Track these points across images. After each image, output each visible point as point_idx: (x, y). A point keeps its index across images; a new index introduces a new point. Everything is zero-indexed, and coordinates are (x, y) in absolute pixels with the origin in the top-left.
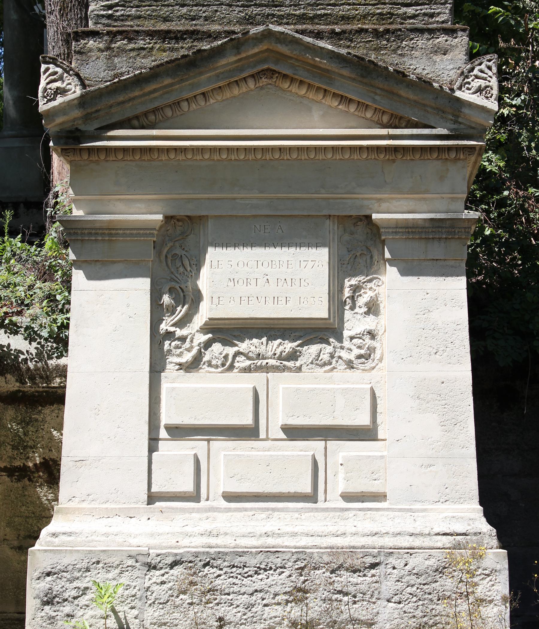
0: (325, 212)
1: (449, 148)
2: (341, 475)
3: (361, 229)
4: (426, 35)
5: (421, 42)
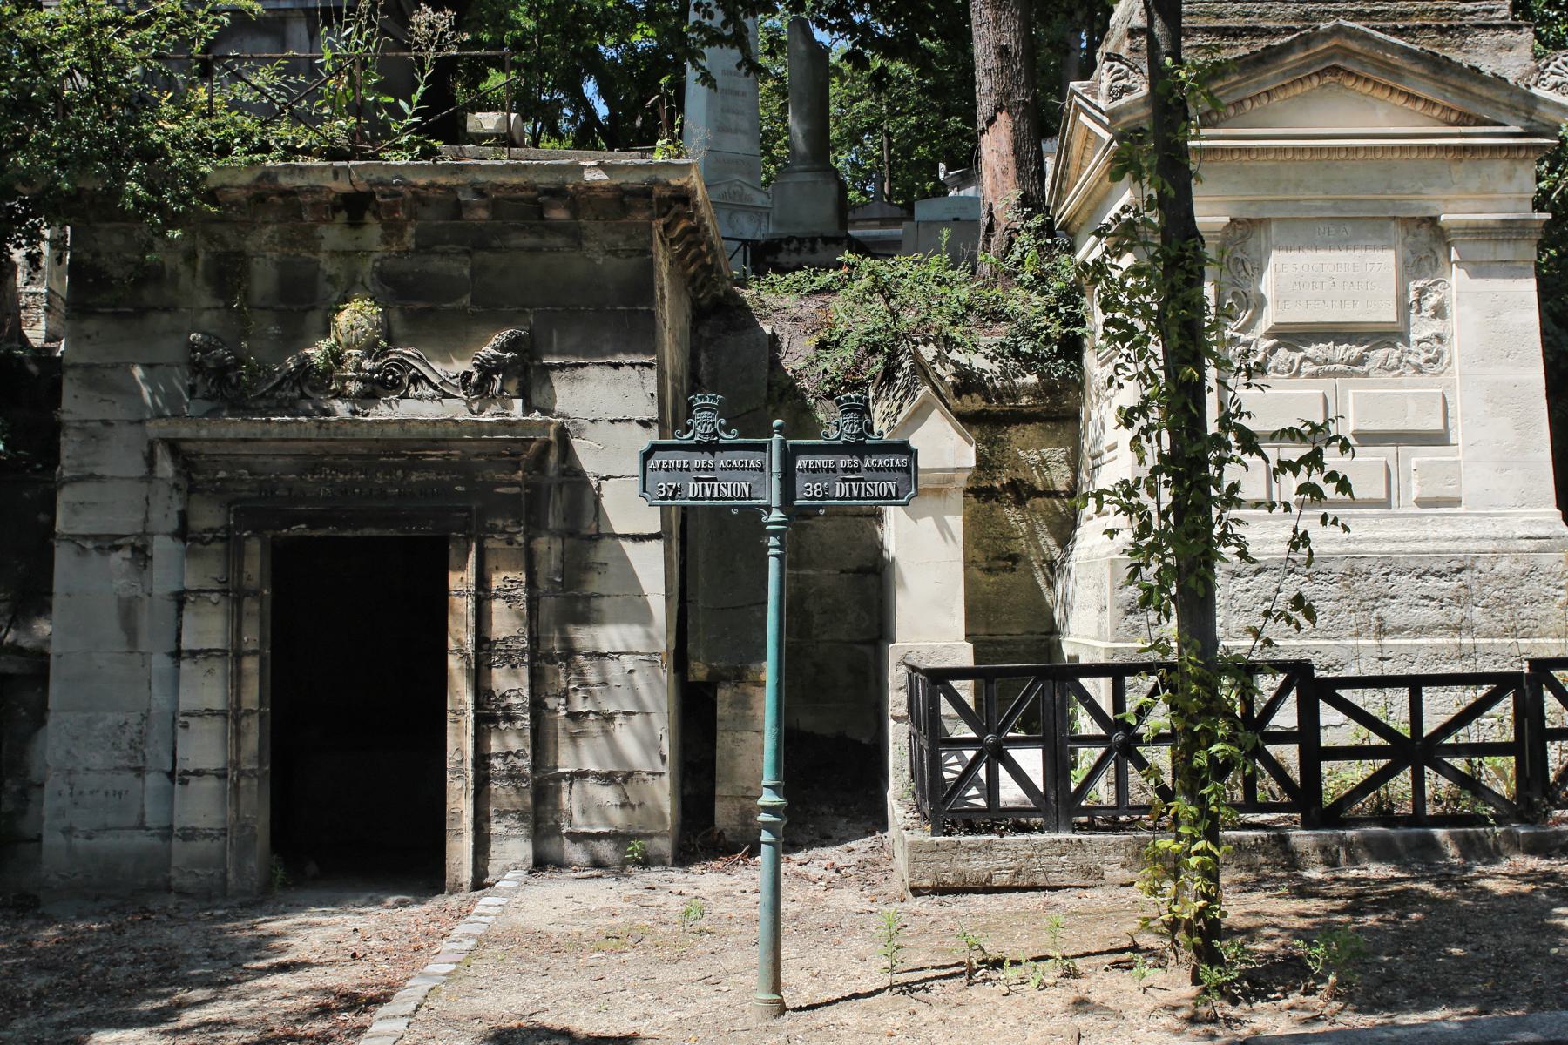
0: (1391, 214)
1: (1519, 147)
2: (1414, 483)
3: (1424, 233)
4: (1491, 32)
5: (1486, 37)
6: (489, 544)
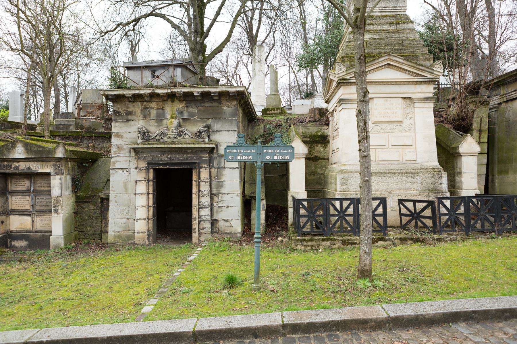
6: (201, 170)
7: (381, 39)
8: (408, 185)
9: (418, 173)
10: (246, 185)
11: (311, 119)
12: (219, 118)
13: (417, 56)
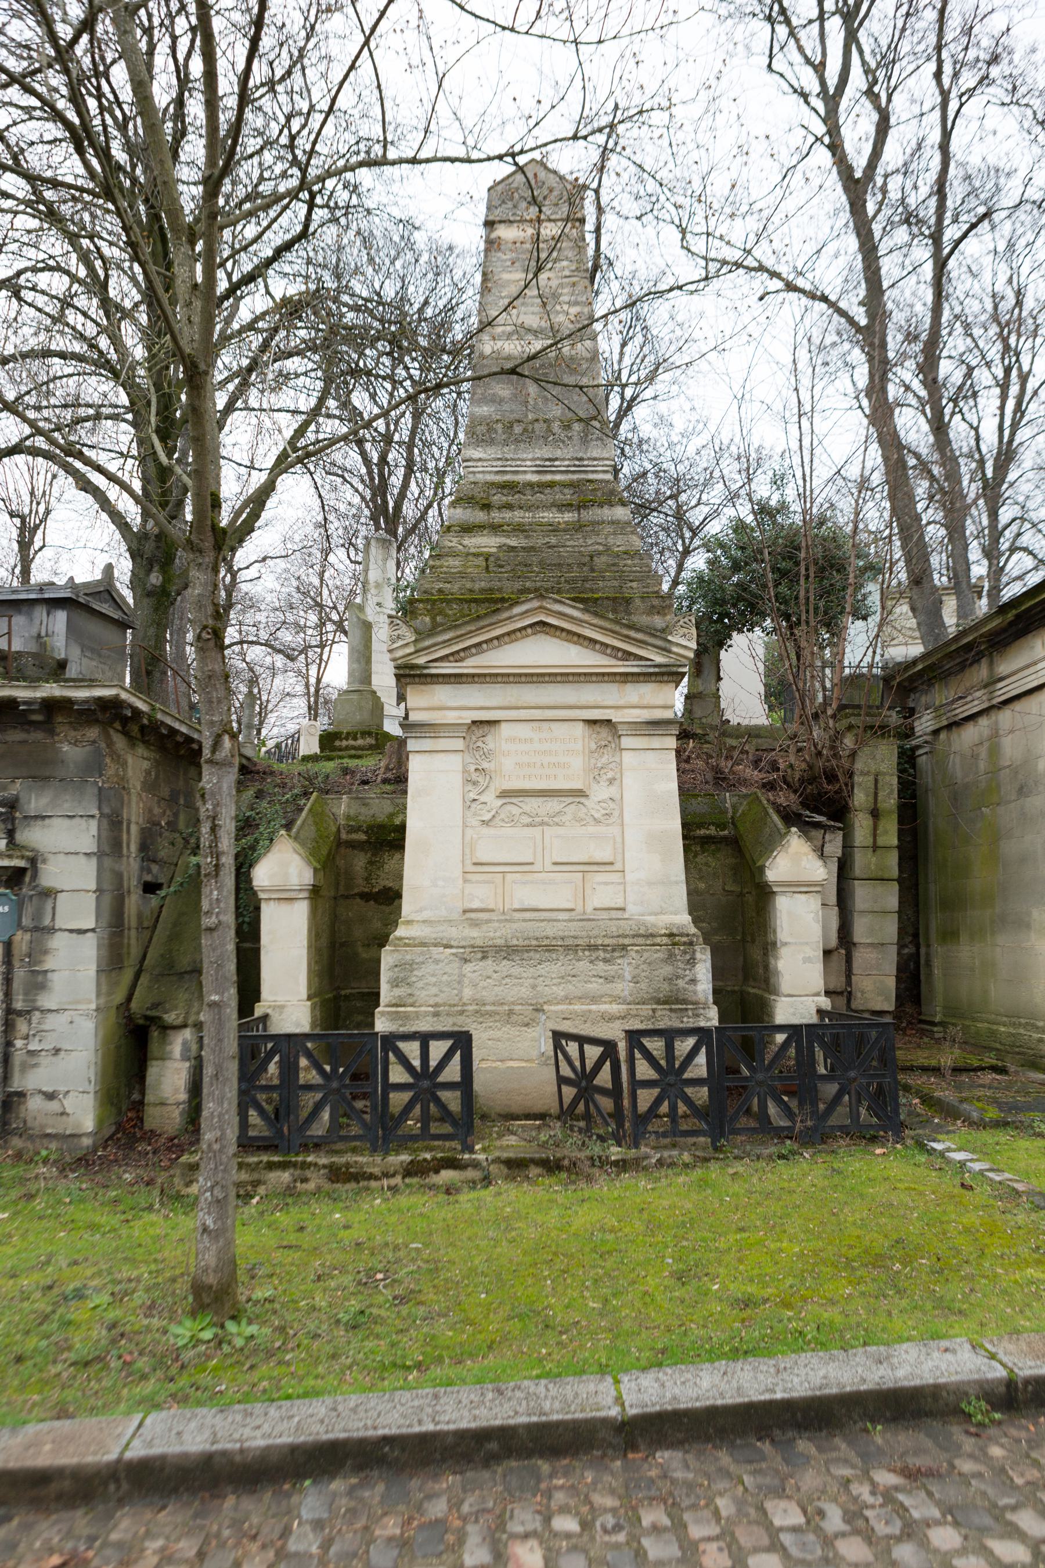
7: (532, 549)
8: (595, 986)
9: (624, 947)
10: (144, 980)
11: (389, 775)
12: (46, 779)
13: (628, 601)
